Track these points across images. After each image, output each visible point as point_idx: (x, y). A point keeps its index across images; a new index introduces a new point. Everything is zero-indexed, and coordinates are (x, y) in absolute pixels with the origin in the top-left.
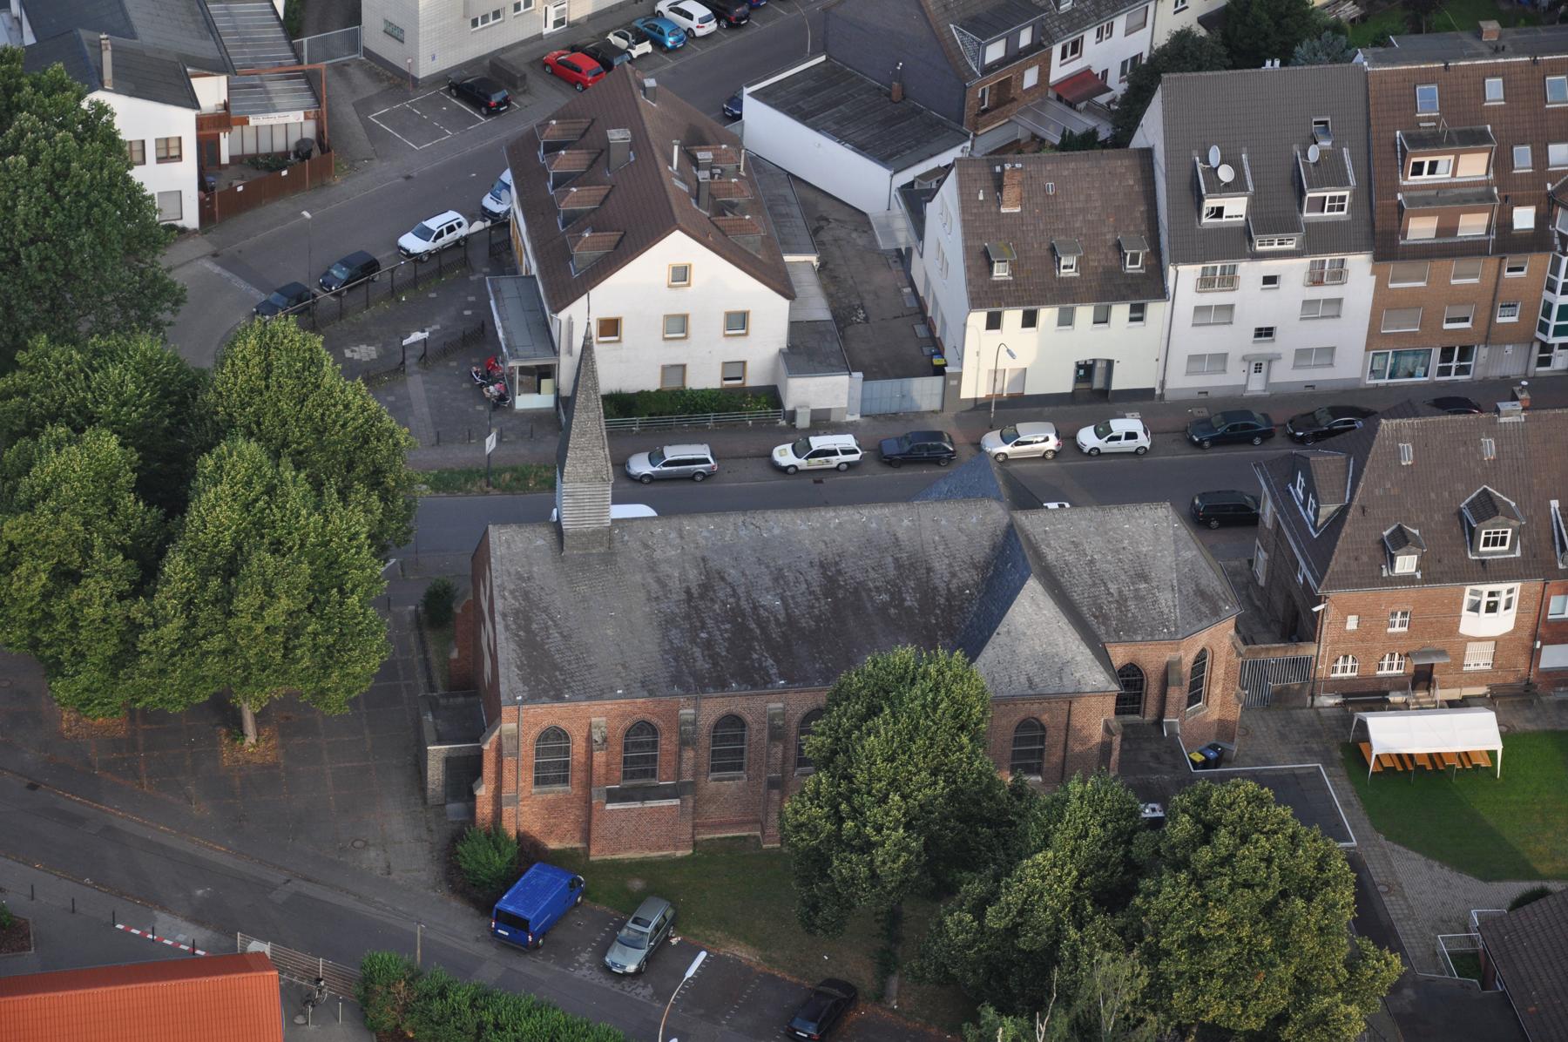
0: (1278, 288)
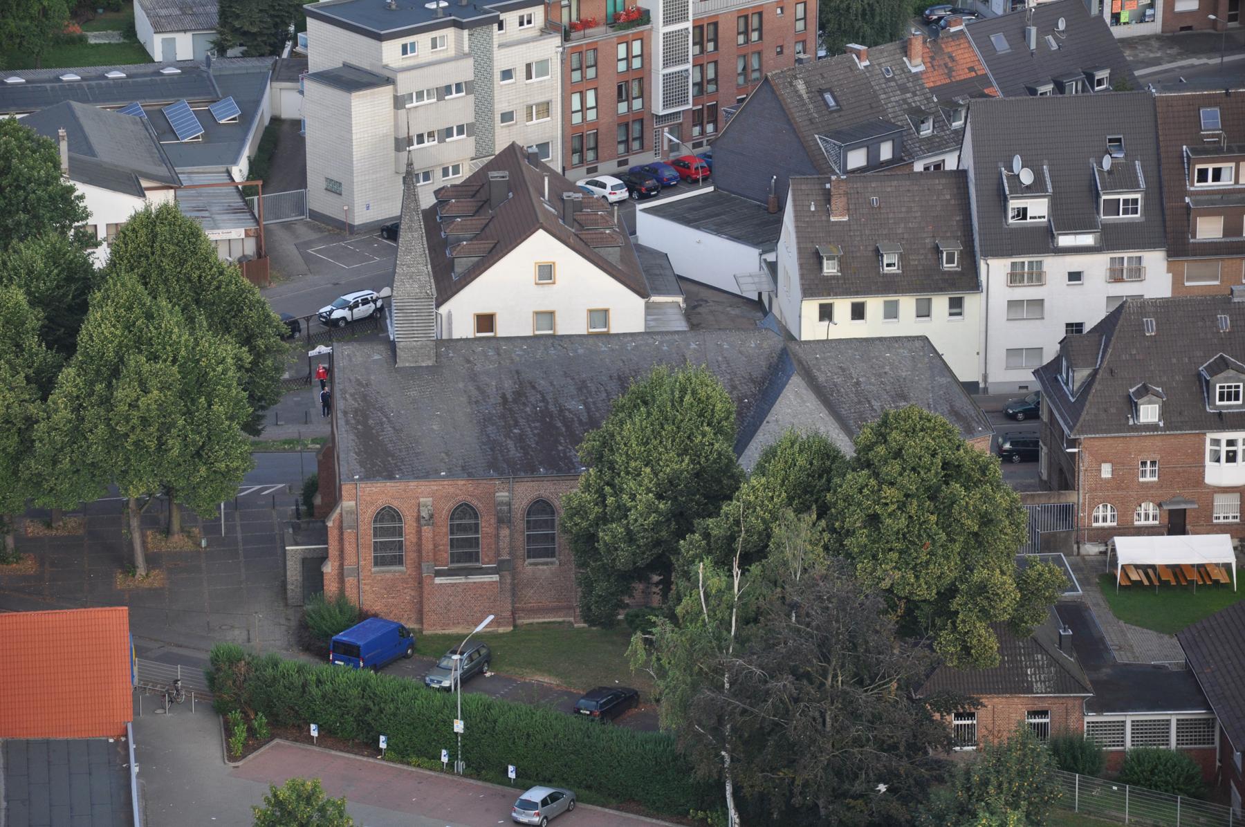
0: (1082, 284)
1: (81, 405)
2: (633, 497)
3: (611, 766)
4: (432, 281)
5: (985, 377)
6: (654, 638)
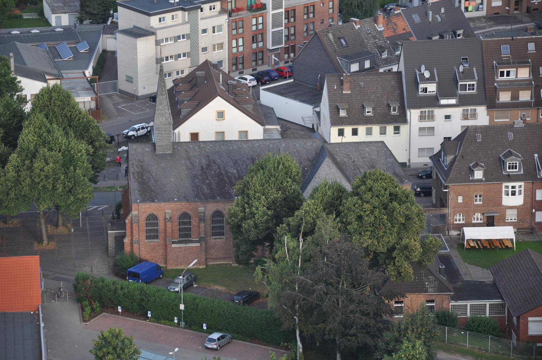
0: (451, 121)
1: (19, 170)
2: (257, 209)
3: (247, 324)
4: (171, 117)
5: (409, 160)
6: (266, 268)
